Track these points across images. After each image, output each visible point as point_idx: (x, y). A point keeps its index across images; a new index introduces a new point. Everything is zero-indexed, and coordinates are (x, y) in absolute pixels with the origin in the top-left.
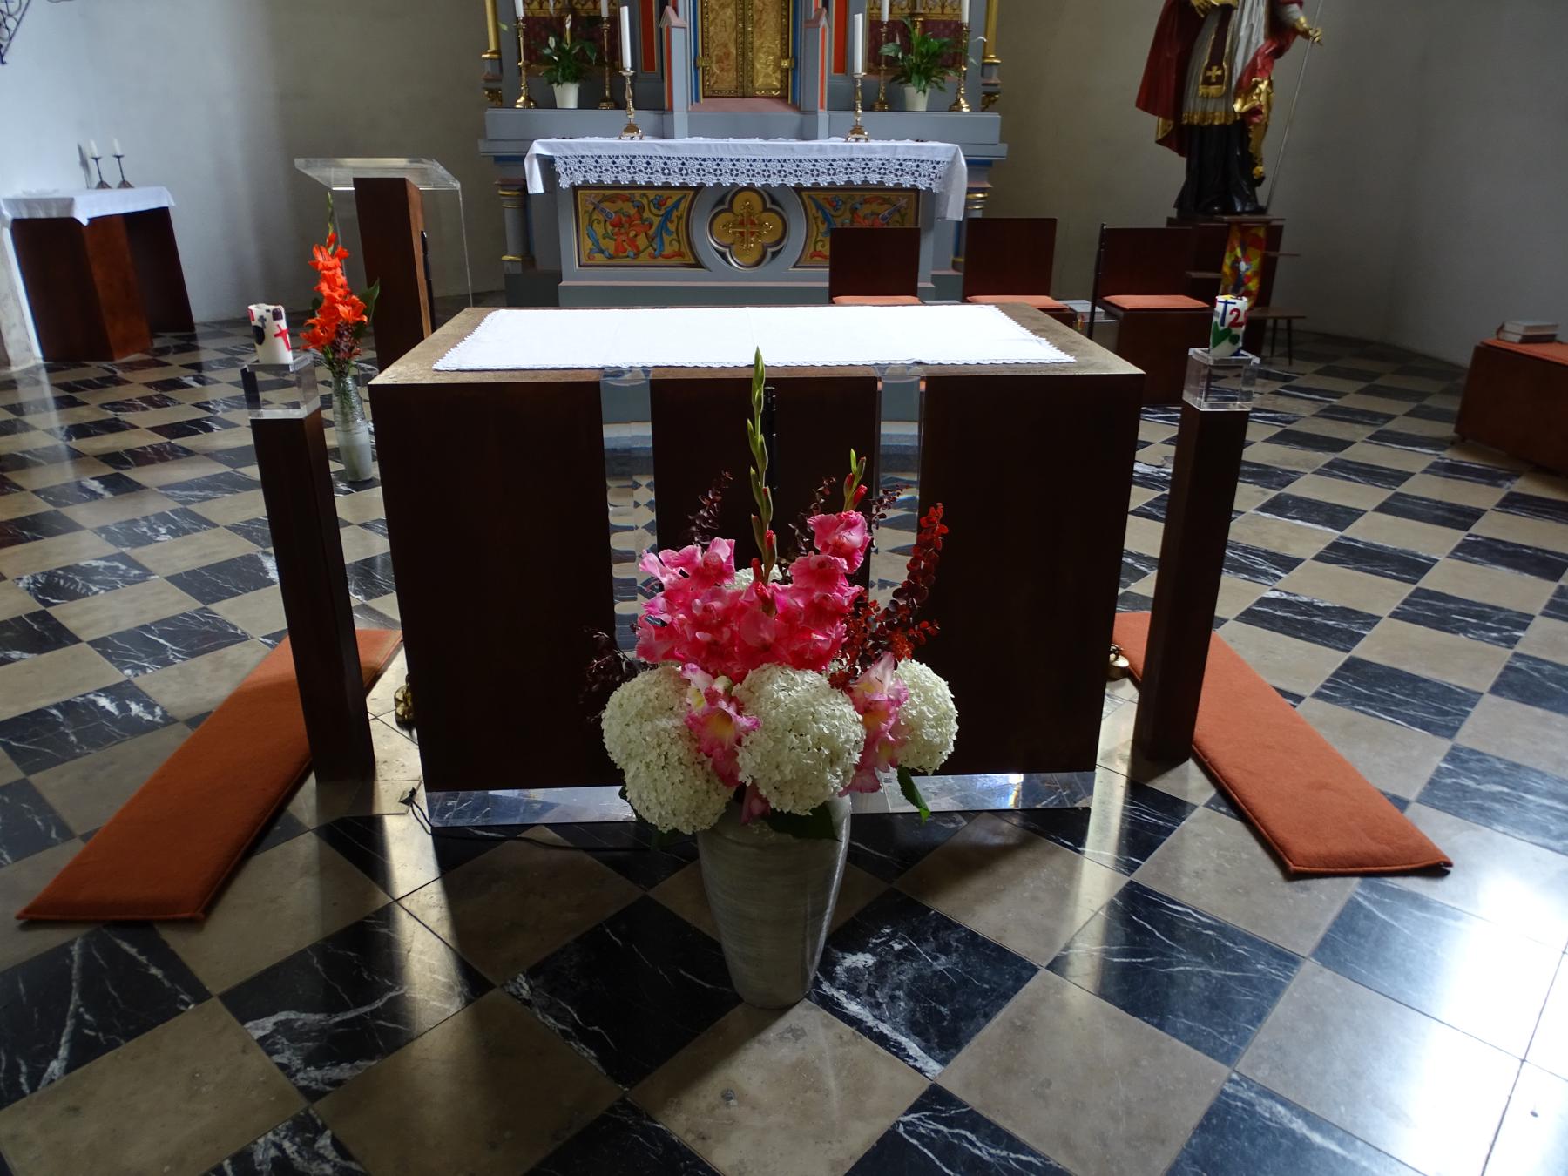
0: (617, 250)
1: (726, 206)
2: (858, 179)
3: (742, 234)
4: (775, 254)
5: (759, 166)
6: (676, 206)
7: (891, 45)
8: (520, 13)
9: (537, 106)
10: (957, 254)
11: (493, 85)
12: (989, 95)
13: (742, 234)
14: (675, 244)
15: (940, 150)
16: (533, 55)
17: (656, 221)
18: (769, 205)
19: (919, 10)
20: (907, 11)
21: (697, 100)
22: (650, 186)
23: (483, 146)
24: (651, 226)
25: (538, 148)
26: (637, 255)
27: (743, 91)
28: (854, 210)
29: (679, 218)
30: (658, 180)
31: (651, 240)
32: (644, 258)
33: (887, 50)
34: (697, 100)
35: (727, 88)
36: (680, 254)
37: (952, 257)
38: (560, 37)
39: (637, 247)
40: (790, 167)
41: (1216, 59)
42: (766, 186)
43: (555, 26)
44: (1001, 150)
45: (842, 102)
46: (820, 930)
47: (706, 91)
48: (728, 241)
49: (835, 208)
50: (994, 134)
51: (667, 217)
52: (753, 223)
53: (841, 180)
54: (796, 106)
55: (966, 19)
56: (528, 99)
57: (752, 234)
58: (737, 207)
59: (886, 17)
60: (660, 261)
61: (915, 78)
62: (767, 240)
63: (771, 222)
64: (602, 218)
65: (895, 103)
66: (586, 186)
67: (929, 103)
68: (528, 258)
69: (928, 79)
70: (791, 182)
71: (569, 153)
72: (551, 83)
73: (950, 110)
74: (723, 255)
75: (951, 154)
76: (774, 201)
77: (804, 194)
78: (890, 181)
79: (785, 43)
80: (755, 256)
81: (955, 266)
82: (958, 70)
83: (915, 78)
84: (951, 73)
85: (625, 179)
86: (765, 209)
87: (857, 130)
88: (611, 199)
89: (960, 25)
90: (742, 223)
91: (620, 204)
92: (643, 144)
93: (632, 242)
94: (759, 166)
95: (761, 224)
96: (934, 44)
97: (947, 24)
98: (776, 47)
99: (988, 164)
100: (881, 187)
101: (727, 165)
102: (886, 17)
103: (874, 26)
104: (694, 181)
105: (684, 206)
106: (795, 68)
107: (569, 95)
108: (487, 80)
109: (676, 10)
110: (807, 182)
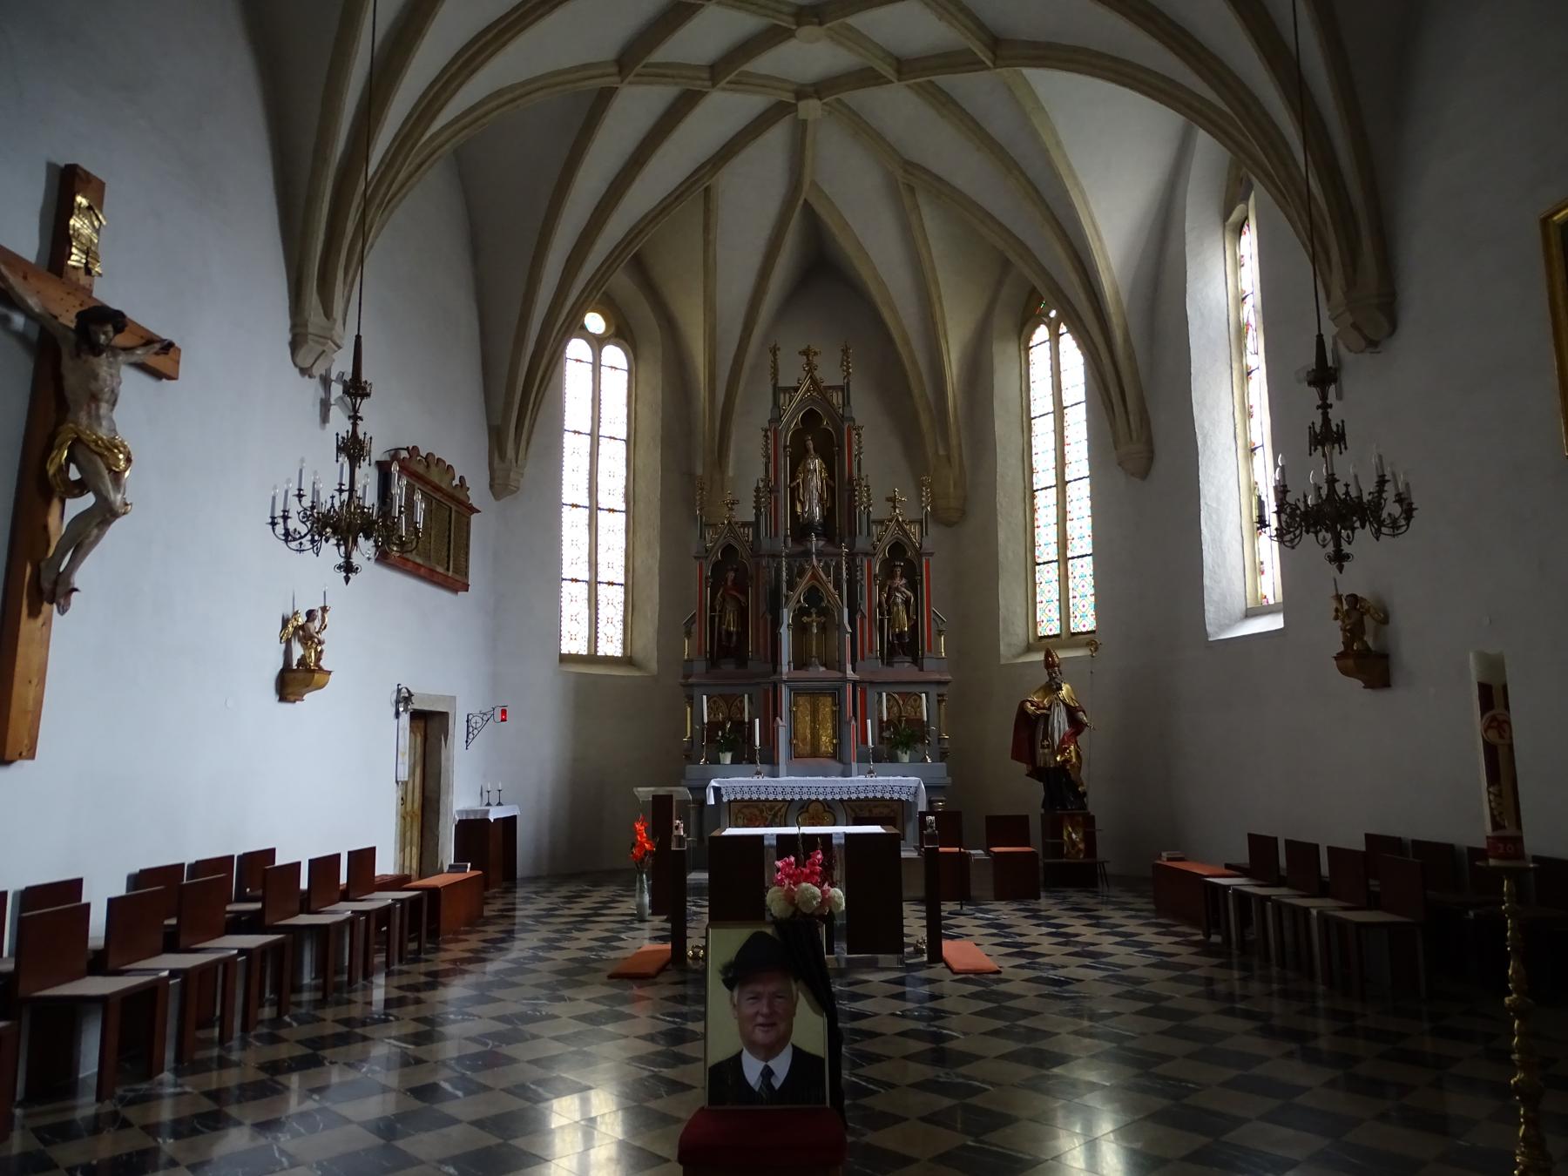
22: (767, 800)
25: (713, 783)
27: (815, 753)
30: (771, 797)
33: (886, 734)
35: (808, 754)
38: (723, 729)
41: (1045, 737)
43: (721, 726)
45: (862, 758)
47: (795, 754)
53: (862, 796)
54: (841, 761)
65: (893, 759)
78: (887, 796)
85: (755, 797)
98: (830, 731)
104: (789, 798)
106: (840, 743)
107: (727, 758)
110: (845, 797)
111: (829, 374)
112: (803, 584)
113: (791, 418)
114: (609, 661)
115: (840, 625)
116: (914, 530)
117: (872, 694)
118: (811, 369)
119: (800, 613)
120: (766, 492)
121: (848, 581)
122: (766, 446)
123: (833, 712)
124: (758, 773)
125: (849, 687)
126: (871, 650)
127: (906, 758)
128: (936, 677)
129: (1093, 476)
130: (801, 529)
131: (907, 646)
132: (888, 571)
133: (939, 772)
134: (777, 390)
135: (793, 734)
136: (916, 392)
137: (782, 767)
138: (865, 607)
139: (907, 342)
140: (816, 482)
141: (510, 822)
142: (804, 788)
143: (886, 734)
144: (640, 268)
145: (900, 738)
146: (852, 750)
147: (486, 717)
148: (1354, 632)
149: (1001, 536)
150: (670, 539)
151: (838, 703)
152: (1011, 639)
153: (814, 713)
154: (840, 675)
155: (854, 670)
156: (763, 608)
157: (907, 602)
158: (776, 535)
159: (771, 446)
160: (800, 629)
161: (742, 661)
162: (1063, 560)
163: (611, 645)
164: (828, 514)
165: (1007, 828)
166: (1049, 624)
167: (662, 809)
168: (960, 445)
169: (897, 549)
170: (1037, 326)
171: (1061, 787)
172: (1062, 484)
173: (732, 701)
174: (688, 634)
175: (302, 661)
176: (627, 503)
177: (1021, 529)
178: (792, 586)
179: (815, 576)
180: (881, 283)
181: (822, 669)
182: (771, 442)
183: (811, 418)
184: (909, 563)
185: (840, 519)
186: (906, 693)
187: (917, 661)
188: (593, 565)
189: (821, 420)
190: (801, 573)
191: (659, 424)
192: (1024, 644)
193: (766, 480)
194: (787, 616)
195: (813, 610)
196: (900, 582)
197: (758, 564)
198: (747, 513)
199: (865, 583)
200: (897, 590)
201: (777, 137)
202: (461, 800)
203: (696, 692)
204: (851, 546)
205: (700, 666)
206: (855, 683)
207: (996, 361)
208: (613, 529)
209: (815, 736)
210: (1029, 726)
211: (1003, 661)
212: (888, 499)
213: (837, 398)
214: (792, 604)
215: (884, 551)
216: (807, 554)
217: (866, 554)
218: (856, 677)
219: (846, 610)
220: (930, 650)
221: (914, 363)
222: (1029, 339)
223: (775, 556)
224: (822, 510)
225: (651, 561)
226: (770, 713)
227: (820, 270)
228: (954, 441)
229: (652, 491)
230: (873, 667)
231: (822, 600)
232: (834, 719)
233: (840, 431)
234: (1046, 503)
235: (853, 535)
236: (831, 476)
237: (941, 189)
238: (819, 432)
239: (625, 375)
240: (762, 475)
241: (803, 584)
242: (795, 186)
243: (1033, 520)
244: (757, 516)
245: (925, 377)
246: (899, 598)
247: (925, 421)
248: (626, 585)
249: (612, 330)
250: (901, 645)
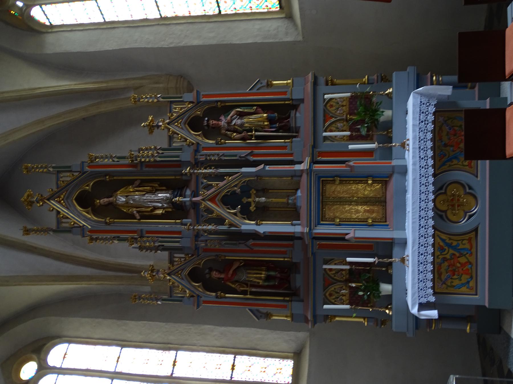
0: (467, 274)
1: (444, 214)
2: (430, 144)
3: (458, 206)
4: (470, 188)
5: (423, 197)
6: (443, 240)
7: (361, 130)
8: (348, 307)
9: (391, 304)
10: (466, 87)
11: (379, 323)
12: (382, 79)
13: (458, 206)
14: (464, 242)
16: (365, 304)
17: (451, 251)
18: (443, 191)
19: (344, 117)
20: (345, 123)
21: (387, 225)
22: (433, 254)
23: (410, 335)
24: (454, 254)
25: (414, 311)
26: (470, 263)
27: (380, 201)
28: (446, 145)
29: (450, 239)
30: (430, 250)
31: (461, 255)
32: (472, 259)
33: (364, 132)
34: (387, 225)
35: (384, 206)
36: (470, 240)
37: (468, 90)
38: (357, 289)
39: (466, 263)
40: (424, 180)
42: (434, 192)
43: (353, 291)
44: (411, 70)
45: (387, 153)
47: (382, 221)
48: (462, 213)
49: (445, 155)
50: (403, 74)
51: (450, 246)
52: (452, 200)
53: (430, 153)
54: (390, 176)
55: (349, 94)
56: (387, 308)
57: (458, 200)
58: (444, 208)
59: (348, 133)
60: (474, 250)
61: (376, 117)
62: (462, 192)
63: (453, 190)
64: (450, 281)
65: (388, 125)
66: (433, 288)
67: (389, 109)
68: (467, 319)
69: (376, 110)
70: (431, 179)
71: (417, 295)
72: (379, 297)
73: (391, 98)
74: (470, 216)
75: (417, 95)
76: (441, 188)
77: (437, 172)
78: (431, 127)
79: (360, 182)
80: (471, 199)
81: (473, 88)
82: (372, 96)
83: (376, 117)
84: (374, 99)
85: (430, 267)
86: (445, 193)
87: (403, 145)
88: (440, 275)
89: (352, 97)
90: (453, 206)
91: (443, 270)
92: (410, 251)
93: (463, 265)
94: (423, 197)
95: (453, 195)
96: (361, 109)
97: (350, 103)
98: (360, 186)
99: (418, 76)
100: (433, 132)
101: (423, 213)
102: (348, 133)
103: (352, 139)
104: (431, 231)
105: (444, 237)
106: (372, 176)
107: (385, 288)
108: (377, 325)
109: (347, 234)
110: (431, 171)
112: (219, 210)
113: (79, 217)
115: (257, 175)
121: (217, 167)
122: (105, 239)
123: (341, 182)
124: (403, 260)
125: (317, 167)
126: (284, 148)
127: (388, 113)
128: (309, 87)
131: (281, 114)
132: (211, 132)
135: (362, 223)
136: (83, 114)
137: (395, 234)
138: (244, 153)
139: (41, 121)
143: (364, 132)
145: (370, 120)
149: (196, 42)
152: (282, 33)
153: (342, 201)
154: (305, 176)
155: (300, 163)
156: (242, 247)
157: (241, 115)
158: (179, 233)
159: (105, 236)
160: (262, 213)
164: (165, 185)
168: (126, 80)
169: (194, 124)
170: (32, 18)
173: (329, 279)
174: (268, 316)
176: (169, 349)
177: (191, 26)
178: (221, 221)
179: (212, 200)
181: (299, 193)
182: (100, 236)
183: (85, 201)
184: (206, 113)
186: (325, 114)
187: (294, 105)
189: (85, 191)
190: (209, 211)
191: (109, 322)
192: (286, 22)
193: (133, 240)
194: (248, 226)
195: (245, 200)
196: (223, 122)
197: (206, 250)
199: (221, 152)
200: (229, 123)
203: (319, 312)
204: (187, 164)
205: (297, 307)
206: (314, 162)
207: (58, 50)
209: (365, 201)
211: (300, 38)
212: (151, 131)
213: (67, 177)
214: (237, 220)
215: (194, 137)
216: (196, 205)
217: (197, 151)
218: (308, 160)
219: (244, 170)
220: (285, 93)
221: (59, 116)
222: (43, 25)
224: (161, 191)
225: (215, 332)
226: (341, 245)
228: (122, 84)
230: (299, 146)
231: (234, 193)
232: (347, 182)
233: (93, 175)
236: (131, 183)
239: (72, 346)
240: (126, 244)
241: (219, 210)
243: (184, 17)
244: (164, 249)
245: (73, 107)
248: (236, 354)
249: (34, 356)
250: (280, 120)
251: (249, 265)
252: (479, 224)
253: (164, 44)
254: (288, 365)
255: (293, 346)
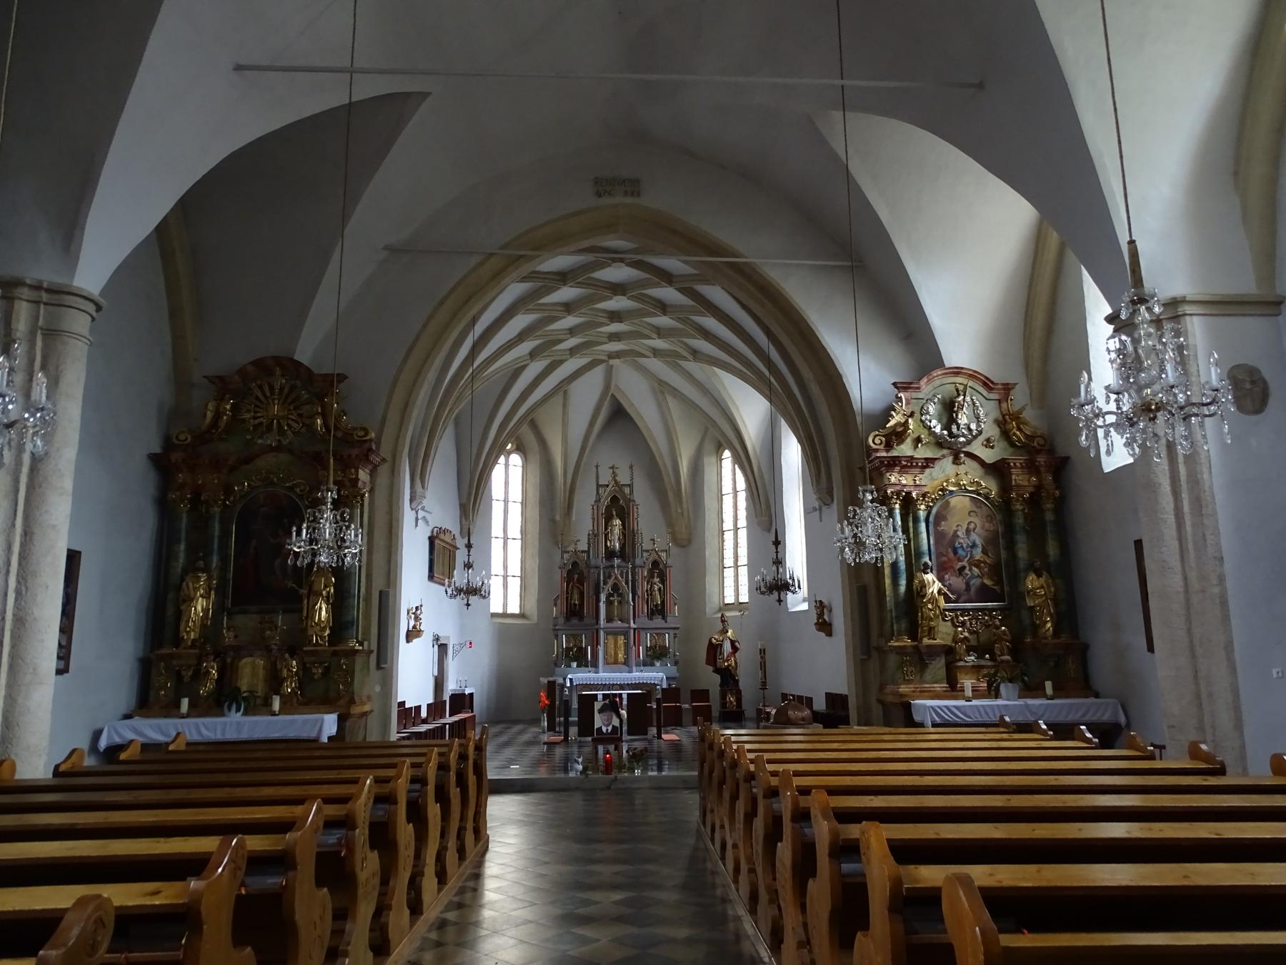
15: (661, 674)
27: (616, 662)
35: (612, 662)
43: (571, 649)
46: (1035, 928)
47: (607, 663)
65: (653, 665)
92: (592, 675)
107: (574, 665)
111: (623, 478)
112: (611, 582)
113: (605, 502)
114: (513, 616)
116: (663, 555)
117: (642, 633)
118: (614, 475)
119: (609, 595)
120: (593, 536)
127: (658, 664)
129: (748, 527)
130: (610, 554)
131: (659, 611)
133: (673, 670)
134: (598, 486)
135: (606, 653)
138: (640, 593)
140: (617, 531)
141: (471, 695)
142: (611, 674)
144: (534, 425)
145: (656, 654)
146: (633, 661)
147: (462, 645)
148: (820, 615)
150: (544, 555)
151: (627, 638)
152: (712, 603)
160: (609, 603)
161: (581, 618)
162: (736, 566)
163: (514, 608)
164: (623, 547)
165: (702, 695)
166: (730, 599)
167: (551, 685)
169: (655, 564)
171: (728, 678)
172: (736, 529)
175: (414, 627)
178: (605, 583)
180: (649, 430)
183: (614, 499)
185: (627, 552)
186: (659, 633)
187: (664, 618)
188: (505, 567)
190: (610, 577)
196: (656, 580)
198: (583, 546)
201: (599, 371)
202: (451, 686)
205: (561, 620)
208: (515, 548)
209: (616, 654)
210: (714, 649)
213: (627, 490)
223: (597, 567)
225: (534, 565)
227: (617, 417)
228: (685, 506)
229: (534, 529)
230: (643, 621)
234: (729, 537)
235: (634, 557)
237: (675, 392)
238: (617, 506)
241: (611, 582)
242: (607, 386)
246: (656, 588)
247: (671, 495)
251: (581, 594)
252: (411, 926)
253: (707, 534)
254: (517, 611)
255: (528, 612)
